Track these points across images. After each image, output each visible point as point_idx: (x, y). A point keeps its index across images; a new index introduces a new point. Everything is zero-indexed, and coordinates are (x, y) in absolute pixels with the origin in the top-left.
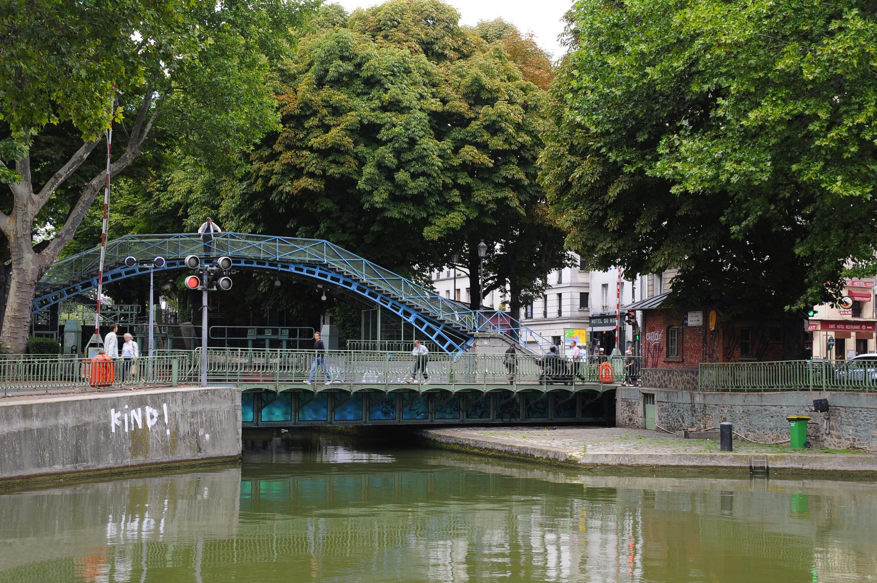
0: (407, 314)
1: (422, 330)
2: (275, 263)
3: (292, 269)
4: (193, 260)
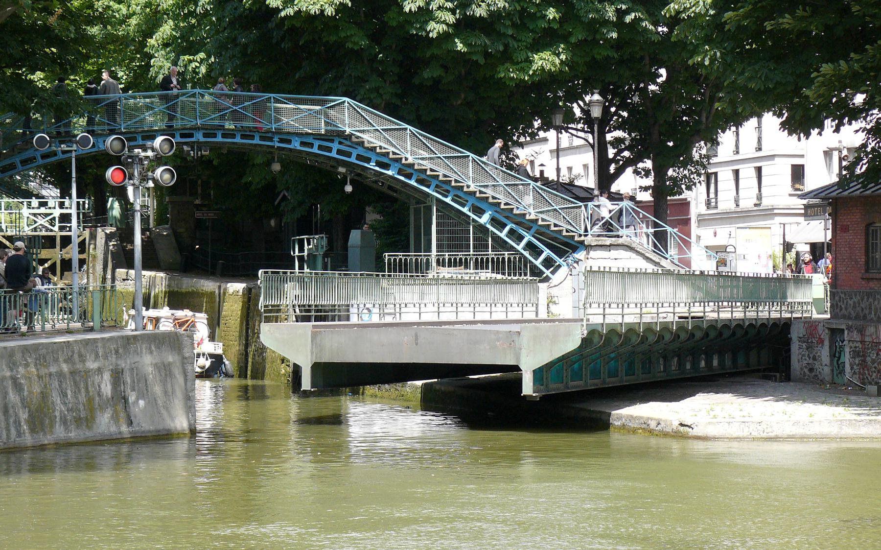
0: (479, 212)
1: (503, 235)
2: (270, 135)
3: (296, 145)
4: (116, 143)
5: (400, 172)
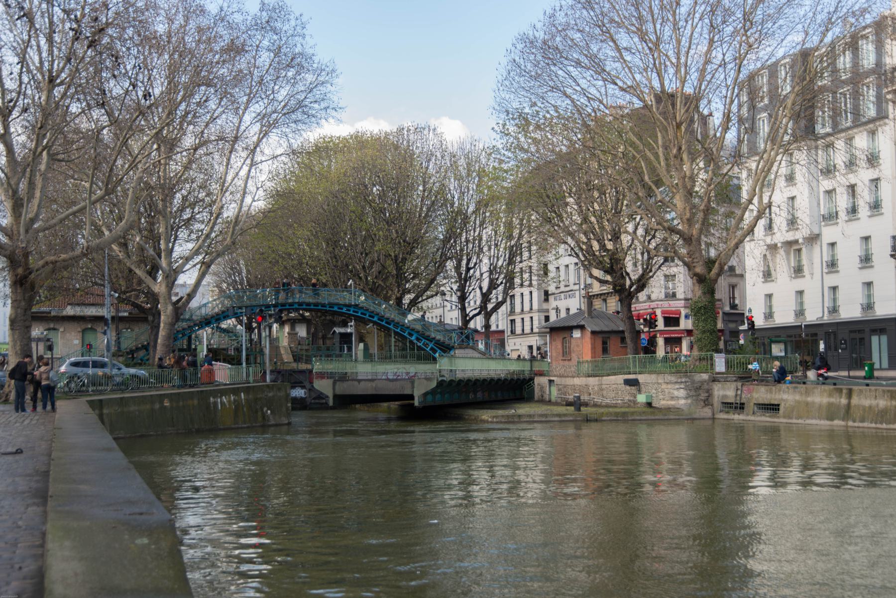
0: (411, 335)
5: (379, 319)
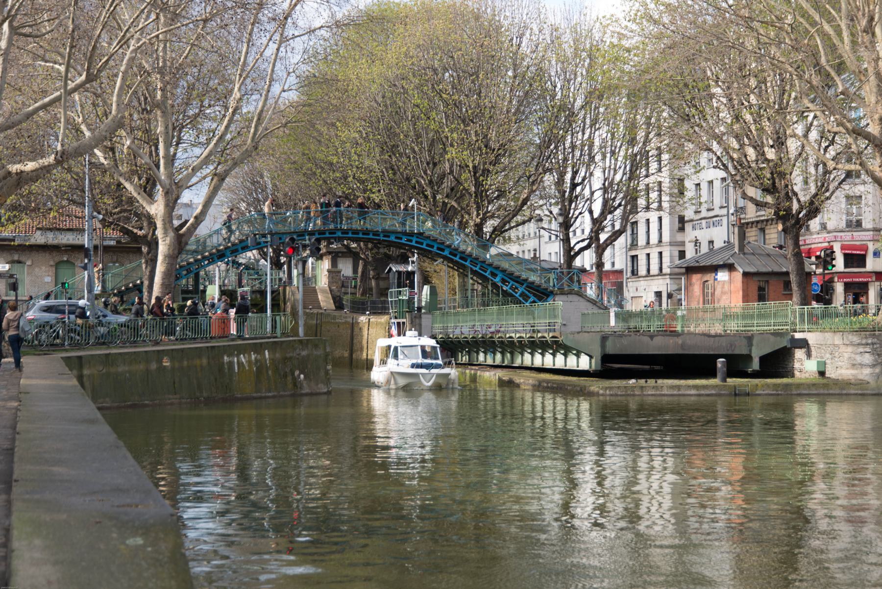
0: (494, 275)
